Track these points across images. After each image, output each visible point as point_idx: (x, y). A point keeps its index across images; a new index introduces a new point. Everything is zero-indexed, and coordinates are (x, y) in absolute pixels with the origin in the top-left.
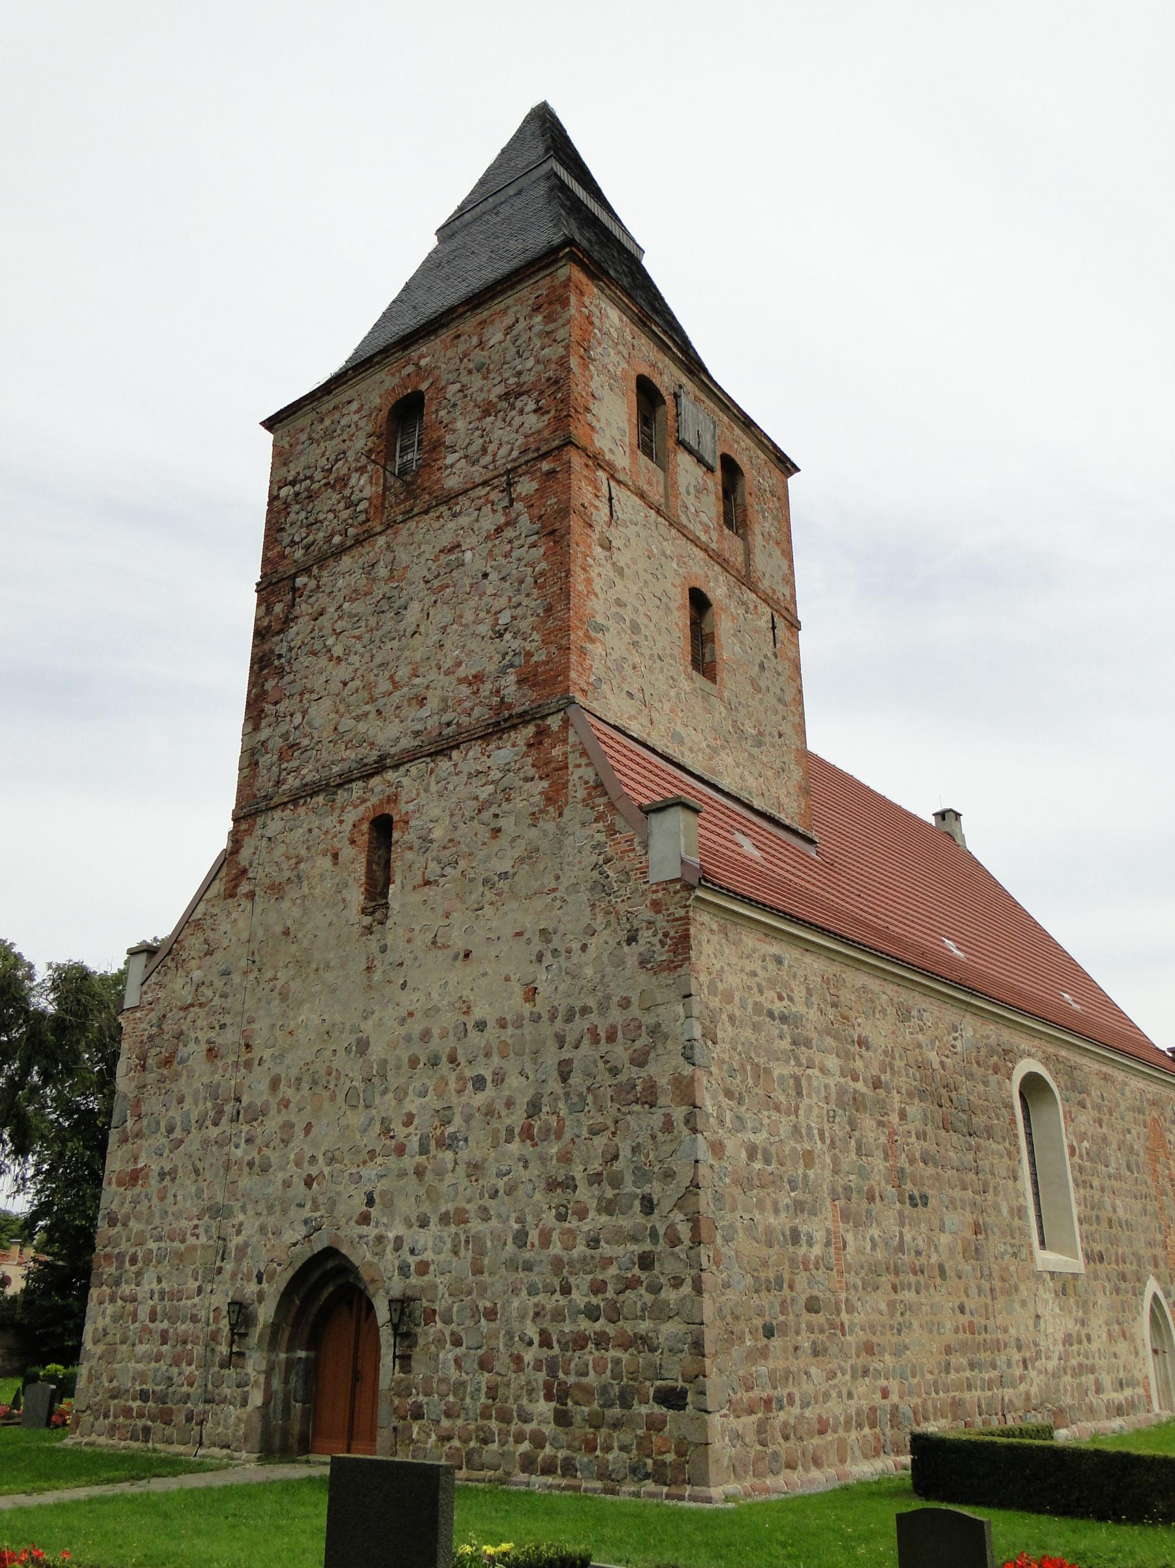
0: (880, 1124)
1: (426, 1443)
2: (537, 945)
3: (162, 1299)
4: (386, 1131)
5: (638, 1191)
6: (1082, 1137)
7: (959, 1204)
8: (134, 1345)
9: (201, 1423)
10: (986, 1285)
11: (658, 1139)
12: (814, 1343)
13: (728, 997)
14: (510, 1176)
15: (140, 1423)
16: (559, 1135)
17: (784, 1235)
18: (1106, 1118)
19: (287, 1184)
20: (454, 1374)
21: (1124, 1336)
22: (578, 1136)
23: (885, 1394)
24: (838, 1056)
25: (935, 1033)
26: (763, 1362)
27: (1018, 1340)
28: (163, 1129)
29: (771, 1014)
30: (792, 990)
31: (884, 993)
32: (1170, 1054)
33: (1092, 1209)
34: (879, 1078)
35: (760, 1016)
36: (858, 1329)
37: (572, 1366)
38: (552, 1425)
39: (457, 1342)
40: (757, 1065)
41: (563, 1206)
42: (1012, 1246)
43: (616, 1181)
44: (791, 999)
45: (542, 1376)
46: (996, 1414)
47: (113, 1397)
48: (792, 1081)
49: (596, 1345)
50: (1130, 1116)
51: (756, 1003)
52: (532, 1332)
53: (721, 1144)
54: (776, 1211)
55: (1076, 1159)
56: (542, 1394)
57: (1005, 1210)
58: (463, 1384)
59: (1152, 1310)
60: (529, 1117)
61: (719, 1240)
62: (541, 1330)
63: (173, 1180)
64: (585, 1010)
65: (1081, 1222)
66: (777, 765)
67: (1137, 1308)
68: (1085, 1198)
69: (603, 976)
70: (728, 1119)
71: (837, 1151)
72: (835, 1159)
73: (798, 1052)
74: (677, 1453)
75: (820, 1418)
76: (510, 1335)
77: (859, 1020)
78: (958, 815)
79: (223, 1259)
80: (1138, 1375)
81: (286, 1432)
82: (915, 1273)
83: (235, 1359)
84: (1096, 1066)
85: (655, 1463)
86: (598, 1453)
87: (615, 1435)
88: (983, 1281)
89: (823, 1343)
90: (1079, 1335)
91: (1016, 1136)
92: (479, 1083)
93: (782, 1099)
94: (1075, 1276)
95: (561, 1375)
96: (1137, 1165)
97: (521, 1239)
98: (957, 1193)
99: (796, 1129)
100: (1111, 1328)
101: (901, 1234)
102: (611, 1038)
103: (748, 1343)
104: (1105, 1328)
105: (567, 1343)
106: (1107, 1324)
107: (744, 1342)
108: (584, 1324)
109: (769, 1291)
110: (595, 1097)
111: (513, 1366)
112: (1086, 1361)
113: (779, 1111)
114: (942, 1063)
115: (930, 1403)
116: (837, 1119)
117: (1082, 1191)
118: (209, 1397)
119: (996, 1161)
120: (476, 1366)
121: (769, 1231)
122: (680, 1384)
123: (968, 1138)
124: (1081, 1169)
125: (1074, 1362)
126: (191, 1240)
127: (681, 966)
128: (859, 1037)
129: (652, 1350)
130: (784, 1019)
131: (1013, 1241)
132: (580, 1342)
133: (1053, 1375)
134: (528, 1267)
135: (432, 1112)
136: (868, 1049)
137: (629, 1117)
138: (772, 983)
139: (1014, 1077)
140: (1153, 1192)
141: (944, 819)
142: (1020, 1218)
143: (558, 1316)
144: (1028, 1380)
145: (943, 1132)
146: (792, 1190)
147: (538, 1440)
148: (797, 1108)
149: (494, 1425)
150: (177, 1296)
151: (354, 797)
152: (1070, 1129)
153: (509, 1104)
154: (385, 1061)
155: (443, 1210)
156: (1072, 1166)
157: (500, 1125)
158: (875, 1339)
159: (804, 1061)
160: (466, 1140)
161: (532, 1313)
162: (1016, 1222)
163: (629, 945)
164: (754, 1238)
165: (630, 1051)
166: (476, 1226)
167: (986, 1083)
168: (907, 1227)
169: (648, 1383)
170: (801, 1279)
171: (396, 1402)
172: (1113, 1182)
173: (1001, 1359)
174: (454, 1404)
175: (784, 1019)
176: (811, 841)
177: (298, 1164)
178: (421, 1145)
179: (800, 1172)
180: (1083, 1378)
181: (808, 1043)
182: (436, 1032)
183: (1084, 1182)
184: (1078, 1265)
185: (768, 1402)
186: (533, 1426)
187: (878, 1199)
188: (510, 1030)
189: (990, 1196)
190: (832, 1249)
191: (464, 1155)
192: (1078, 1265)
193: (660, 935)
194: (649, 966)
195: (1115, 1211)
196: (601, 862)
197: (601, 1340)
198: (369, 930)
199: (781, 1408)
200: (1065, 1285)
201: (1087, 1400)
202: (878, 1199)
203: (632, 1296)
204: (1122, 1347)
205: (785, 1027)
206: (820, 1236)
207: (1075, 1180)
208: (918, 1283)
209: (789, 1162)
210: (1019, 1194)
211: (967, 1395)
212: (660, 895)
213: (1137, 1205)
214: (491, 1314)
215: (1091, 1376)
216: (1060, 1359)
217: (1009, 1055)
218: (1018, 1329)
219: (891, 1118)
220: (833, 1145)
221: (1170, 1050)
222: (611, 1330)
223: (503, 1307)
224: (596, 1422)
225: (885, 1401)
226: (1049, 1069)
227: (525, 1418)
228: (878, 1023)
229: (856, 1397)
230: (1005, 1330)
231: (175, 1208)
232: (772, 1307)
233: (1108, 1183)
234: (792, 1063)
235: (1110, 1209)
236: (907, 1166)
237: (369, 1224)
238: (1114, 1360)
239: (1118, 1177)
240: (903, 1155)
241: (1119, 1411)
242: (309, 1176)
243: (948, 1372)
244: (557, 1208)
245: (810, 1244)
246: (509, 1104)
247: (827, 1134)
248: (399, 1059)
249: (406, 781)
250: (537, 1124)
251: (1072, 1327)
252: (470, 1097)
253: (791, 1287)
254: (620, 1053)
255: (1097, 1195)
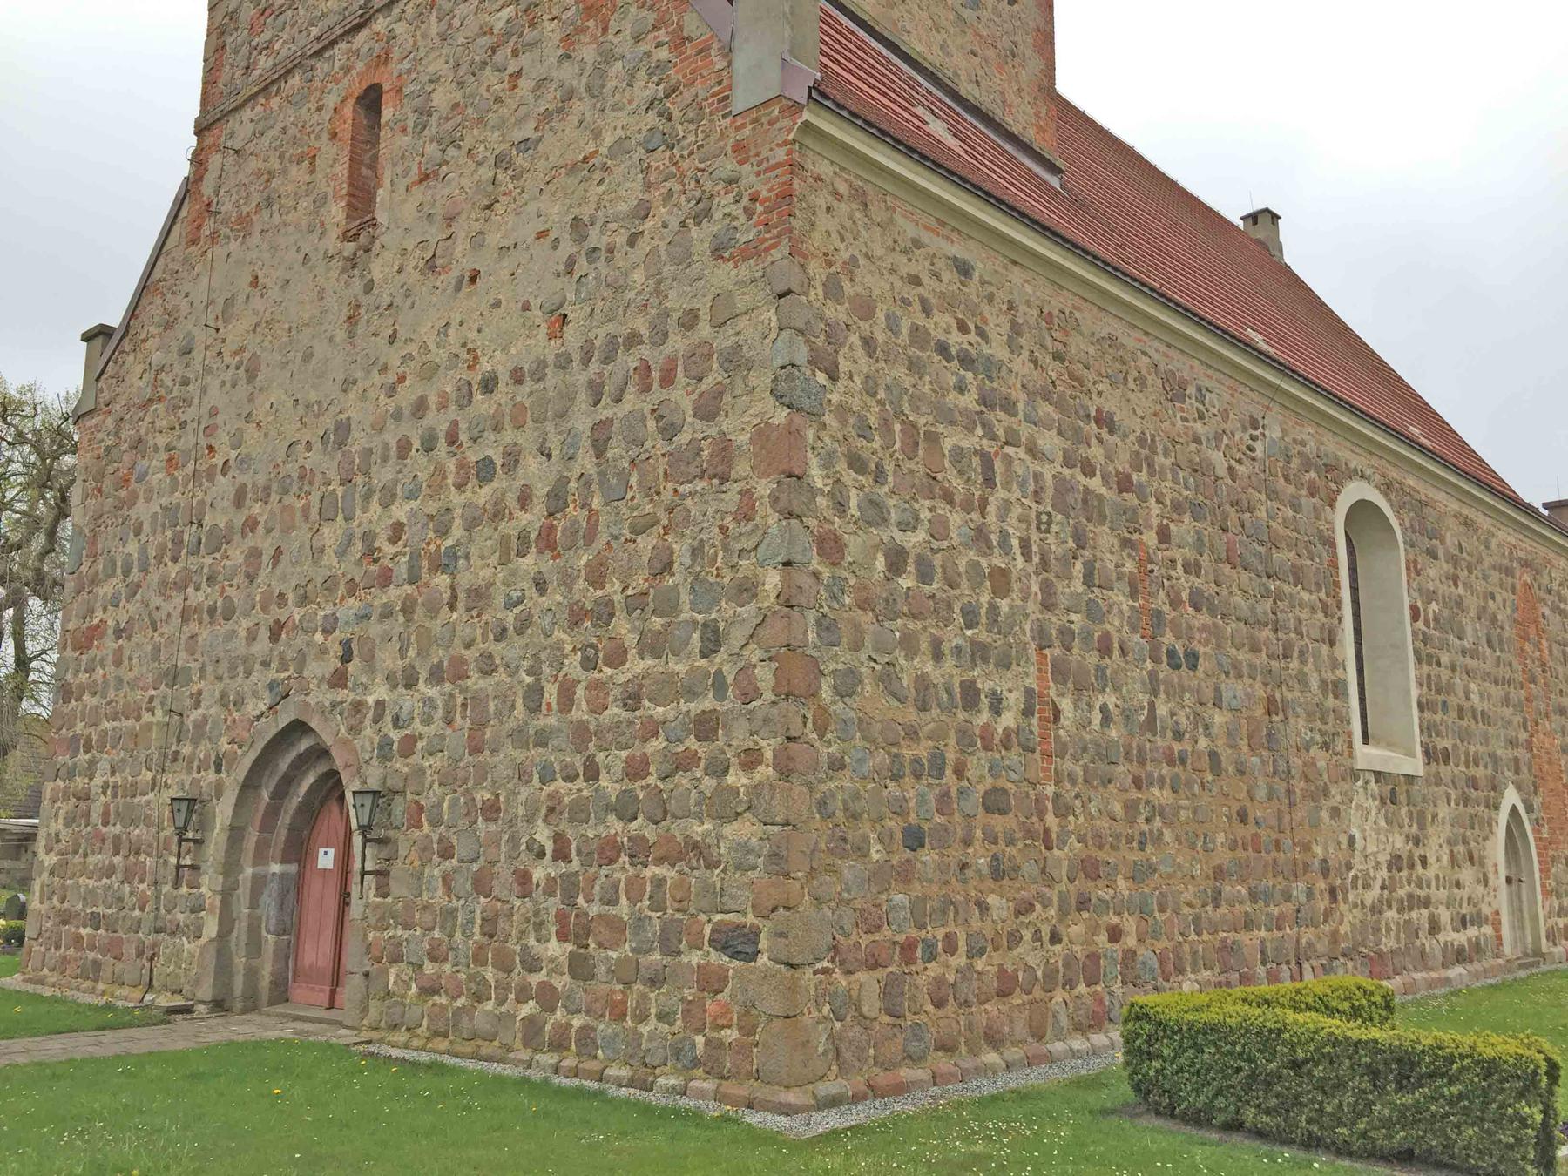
0: (1126, 543)
1: (403, 997)
2: (567, 248)
3: (115, 796)
4: (371, 554)
5: (699, 617)
6: (1430, 596)
7: (1245, 670)
8: (86, 855)
9: (151, 959)
10: (1281, 787)
11: (730, 532)
12: (995, 857)
13: (865, 309)
14: (521, 608)
15: (91, 955)
16: (590, 537)
17: (949, 692)
18: (1463, 575)
19: (252, 637)
20: (438, 897)
21: (1471, 859)
22: (616, 538)
23: (1115, 934)
24: (1060, 433)
25: (1223, 426)
26: (901, 887)
27: (1324, 861)
28: (119, 571)
29: (943, 349)
30: (986, 323)
31: (1145, 353)
32: (1546, 512)
33: (1438, 691)
34: (1128, 477)
35: (923, 349)
36: (1073, 839)
37: (597, 888)
38: (567, 978)
39: (447, 853)
40: (914, 426)
41: (592, 646)
42: (1322, 734)
43: (669, 606)
44: (982, 333)
45: (554, 903)
46: (1288, 963)
47: (65, 923)
48: (976, 461)
49: (631, 856)
50: (1495, 576)
51: (915, 329)
52: (543, 835)
53: (837, 540)
54: (938, 656)
55: (1420, 624)
56: (554, 929)
57: (1314, 684)
58: (452, 913)
59: (1509, 828)
60: (551, 515)
61: (826, 693)
62: (557, 834)
63: (129, 638)
64: (633, 339)
65: (1421, 707)
66: (1005, 43)
67: (1490, 825)
68: (1429, 676)
69: (659, 283)
70: (853, 503)
71: (1051, 576)
72: (1047, 587)
73: (990, 416)
74: (740, 1029)
75: (1002, 971)
76: (514, 841)
77: (1101, 387)
78: (1275, 217)
79: (179, 742)
80: (1486, 910)
81: (252, 974)
82: (1171, 763)
83: (186, 873)
84: (1454, 506)
85: (708, 1043)
86: (629, 1023)
87: (652, 995)
88: (1276, 779)
89: (1012, 858)
90: (1410, 857)
91: (1337, 585)
92: (485, 470)
93: (957, 483)
94: (1410, 779)
95: (580, 901)
96: (1501, 641)
97: (534, 695)
98: (1243, 656)
99: (980, 536)
100: (1456, 849)
101: (1152, 706)
102: (668, 380)
103: (875, 856)
104: (1446, 849)
105: (590, 853)
106: (1449, 842)
107: (867, 855)
108: (615, 825)
109: (918, 777)
110: (642, 476)
111: (517, 889)
112: (1419, 892)
113: (951, 502)
114: (1230, 468)
115: (1187, 948)
116: (1054, 528)
117: (1425, 668)
118: (159, 924)
119: (1303, 616)
120: (469, 886)
121: (922, 682)
122: (750, 919)
123: (1265, 579)
124: (1426, 639)
125: (1401, 893)
126: (147, 717)
127: (774, 246)
128: (1099, 411)
129: (710, 866)
130: (966, 361)
131: (1324, 727)
132: (609, 851)
133: (1373, 909)
134: (542, 740)
135: (424, 520)
136: (1111, 432)
137: (689, 502)
138: (950, 303)
139: (1338, 504)
140: (1519, 677)
141: (1256, 223)
142: (1336, 697)
143: (579, 812)
144: (1336, 916)
145: (1227, 568)
146: (969, 627)
147: (548, 998)
148: (984, 503)
149: (490, 973)
150: (133, 790)
151: (336, 68)
152: (1414, 585)
153: (525, 500)
154: (370, 451)
155: (435, 661)
156: (1414, 633)
157: (508, 528)
158: (1102, 856)
159: (1001, 433)
160: (467, 557)
161: (544, 811)
162: (1331, 702)
163: (698, 224)
164: (894, 695)
165: (694, 397)
166: (475, 682)
167: (1296, 508)
168: (1163, 696)
169: (703, 917)
170: (978, 764)
171: (371, 936)
172: (1468, 660)
173: (1299, 889)
174: (441, 942)
175: (966, 361)
176: (1054, 169)
177: (265, 609)
178: (411, 568)
179: (985, 599)
180: (1414, 914)
181: (1009, 407)
182: (433, 400)
183: (1429, 656)
184: (1414, 765)
185: (908, 948)
186: (541, 976)
187: (1116, 653)
188: (528, 385)
189: (1294, 664)
190: (1035, 721)
191: (465, 580)
192: (1414, 765)
193: (745, 200)
194: (727, 255)
195: (1468, 699)
196: (661, 95)
197: (639, 851)
198: (352, 263)
199: (932, 957)
200: (1393, 790)
201: (1418, 943)
202: (1116, 653)
203: (684, 781)
204: (1467, 874)
205: (969, 375)
206: (1014, 699)
207: (1416, 652)
208: (1176, 777)
209: (965, 584)
210: (1335, 664)
211: (1244, 938)
212: (747, 131)
213: (1497, 692)
214: (491, 811)
215: (1425, 912)
216: (1383, 888)
217: (1336, 473)
218: (1325, 849)
219: (1144, 538)
220: (1044, 564)
221: (1546, 506)
222: (651, 833)
223: (507, 800)
224: (626, 975)
225: (1116, 946)
226: (1389, 500)
227: (532, 965)
228: (1131, 396)
229: (1065, 939)
230: (1307, 848)
231: (131, 675)
232: (922, 800)
233: (1460, 660)
234: (979, 431)
235: (1461, 694)
236: (1166, 609)
237: (345, 687)
238: (1456, 891)
239: (1474, 654)
240: (1162, 594)
241: (1460, 956)
242: (277, 622)
243: (1217, 906)
244: (583, 649)
245: (997, 707)
246: (525, 500)
247: (1035, 548)
248: (386, 446)
249: (400, 28)
250: (561, 524)
251: (1399, 843)
252: (474, 492)
253: (959, 772)
254: (682, 398)
255: (1445, 674)
